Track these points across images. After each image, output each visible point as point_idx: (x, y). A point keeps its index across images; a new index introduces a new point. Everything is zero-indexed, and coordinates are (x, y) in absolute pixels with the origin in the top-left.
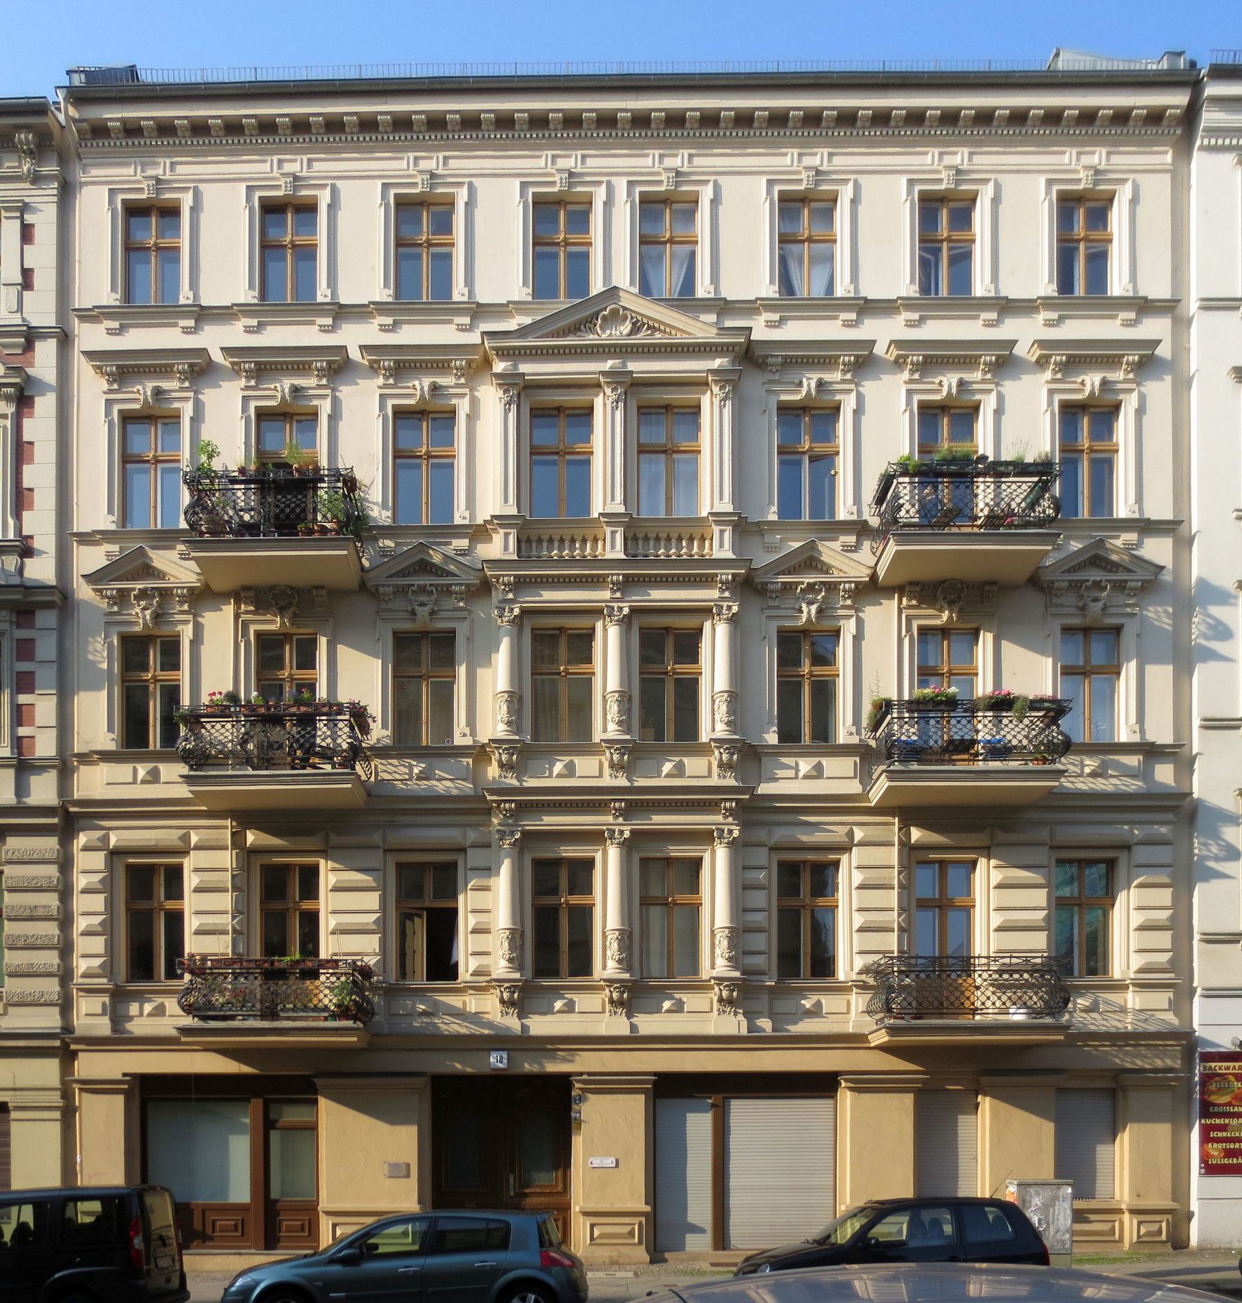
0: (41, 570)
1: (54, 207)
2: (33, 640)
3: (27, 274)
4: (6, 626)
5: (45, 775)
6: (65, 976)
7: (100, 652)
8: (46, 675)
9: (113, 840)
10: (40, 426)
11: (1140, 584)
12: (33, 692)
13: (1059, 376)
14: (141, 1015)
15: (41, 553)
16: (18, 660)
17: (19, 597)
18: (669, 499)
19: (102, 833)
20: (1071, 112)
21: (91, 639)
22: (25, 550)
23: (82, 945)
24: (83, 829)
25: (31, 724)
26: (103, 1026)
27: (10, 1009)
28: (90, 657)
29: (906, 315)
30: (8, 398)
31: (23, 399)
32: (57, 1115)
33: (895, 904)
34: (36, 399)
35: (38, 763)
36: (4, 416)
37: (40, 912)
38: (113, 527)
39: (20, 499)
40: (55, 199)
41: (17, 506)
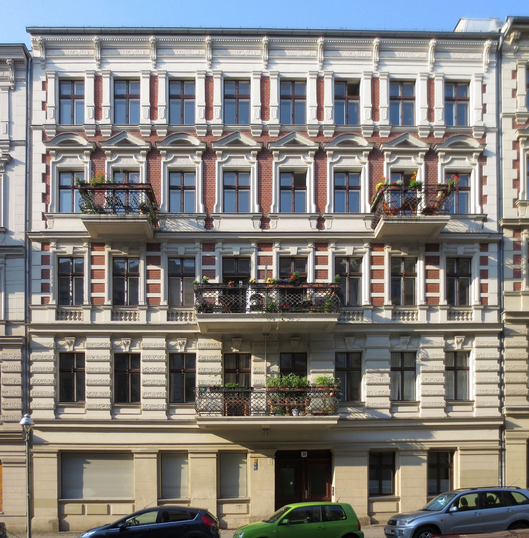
3: (484, 105)
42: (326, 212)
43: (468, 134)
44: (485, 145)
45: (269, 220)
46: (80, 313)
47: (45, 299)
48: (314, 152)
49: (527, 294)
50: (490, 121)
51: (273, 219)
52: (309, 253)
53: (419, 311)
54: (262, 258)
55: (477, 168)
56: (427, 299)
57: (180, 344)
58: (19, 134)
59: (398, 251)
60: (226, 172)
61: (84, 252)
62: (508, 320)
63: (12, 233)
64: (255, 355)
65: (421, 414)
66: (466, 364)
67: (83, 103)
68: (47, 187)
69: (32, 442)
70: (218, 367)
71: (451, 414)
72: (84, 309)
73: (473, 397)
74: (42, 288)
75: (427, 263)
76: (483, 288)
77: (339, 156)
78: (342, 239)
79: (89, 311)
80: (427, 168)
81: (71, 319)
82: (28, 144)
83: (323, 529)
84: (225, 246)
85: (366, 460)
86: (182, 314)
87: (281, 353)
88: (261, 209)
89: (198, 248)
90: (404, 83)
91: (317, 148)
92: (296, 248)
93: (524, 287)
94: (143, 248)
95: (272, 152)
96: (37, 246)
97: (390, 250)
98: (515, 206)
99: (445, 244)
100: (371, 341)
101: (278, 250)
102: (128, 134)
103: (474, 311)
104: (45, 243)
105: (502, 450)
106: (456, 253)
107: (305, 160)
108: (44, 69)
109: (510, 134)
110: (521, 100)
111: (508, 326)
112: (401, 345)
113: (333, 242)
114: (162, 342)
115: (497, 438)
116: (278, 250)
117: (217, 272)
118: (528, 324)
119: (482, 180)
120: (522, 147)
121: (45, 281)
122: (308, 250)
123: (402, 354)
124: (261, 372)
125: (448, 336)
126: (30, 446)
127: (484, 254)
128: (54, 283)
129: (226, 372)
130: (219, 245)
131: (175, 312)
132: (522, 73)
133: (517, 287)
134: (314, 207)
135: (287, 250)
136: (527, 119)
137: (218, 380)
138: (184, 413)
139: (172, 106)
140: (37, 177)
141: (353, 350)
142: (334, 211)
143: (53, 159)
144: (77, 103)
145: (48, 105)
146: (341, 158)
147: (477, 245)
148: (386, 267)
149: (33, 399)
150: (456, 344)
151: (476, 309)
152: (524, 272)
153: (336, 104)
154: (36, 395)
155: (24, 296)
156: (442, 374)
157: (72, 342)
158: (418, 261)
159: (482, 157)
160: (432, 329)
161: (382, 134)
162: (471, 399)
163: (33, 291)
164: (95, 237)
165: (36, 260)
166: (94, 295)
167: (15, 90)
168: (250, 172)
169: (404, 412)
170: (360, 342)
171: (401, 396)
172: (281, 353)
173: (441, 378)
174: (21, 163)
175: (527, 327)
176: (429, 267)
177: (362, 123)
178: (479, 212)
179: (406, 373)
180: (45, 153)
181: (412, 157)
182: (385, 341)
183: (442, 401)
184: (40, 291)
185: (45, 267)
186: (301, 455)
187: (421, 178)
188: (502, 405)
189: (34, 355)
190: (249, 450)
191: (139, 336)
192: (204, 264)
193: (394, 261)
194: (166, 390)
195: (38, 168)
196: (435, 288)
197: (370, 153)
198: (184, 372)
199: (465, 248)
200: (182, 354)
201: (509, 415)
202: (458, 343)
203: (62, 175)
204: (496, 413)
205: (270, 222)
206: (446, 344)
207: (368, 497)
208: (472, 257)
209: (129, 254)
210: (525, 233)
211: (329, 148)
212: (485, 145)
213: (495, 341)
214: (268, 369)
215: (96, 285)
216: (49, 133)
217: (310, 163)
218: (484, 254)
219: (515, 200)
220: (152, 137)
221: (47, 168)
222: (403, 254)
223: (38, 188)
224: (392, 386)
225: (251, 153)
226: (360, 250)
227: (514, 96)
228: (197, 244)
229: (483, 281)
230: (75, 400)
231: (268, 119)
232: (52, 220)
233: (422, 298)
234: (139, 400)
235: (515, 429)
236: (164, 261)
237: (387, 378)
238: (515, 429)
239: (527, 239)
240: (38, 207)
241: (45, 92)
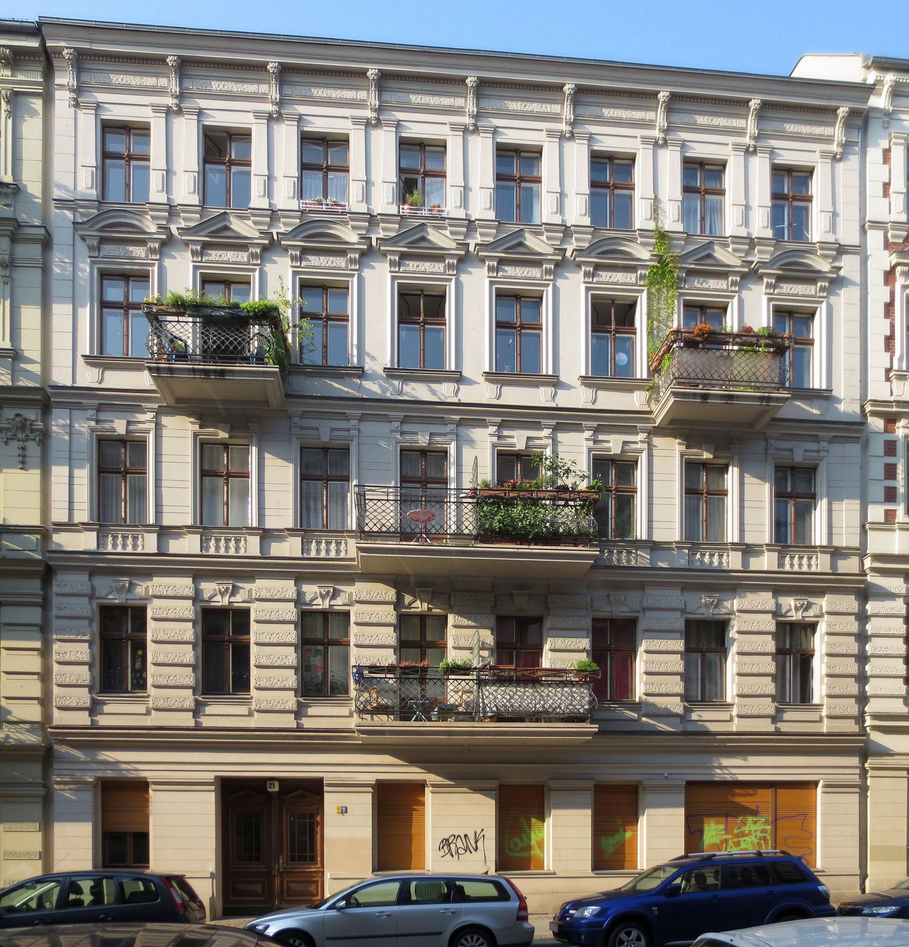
49: (906, 528)
50: (848, 235)
62: (873, 570)
63: (839, 401)
66: (809, 642)
68: (892, 326)
69: (865, 751)
70: (389, 636)
73: (733, 697)
82: (860, 250)
83: (388, 916)
85: (589, 797)
92: (124, 422)
93: (901, 516)
96: (877, 424)
98: (888, 379)
104: (891, 419)
108: (886, 128)
109: (881, 259)
110: (898, 202)
111: (871, 578)
118: (908, 576)
120: (900, 281)
121: (890, 483)
126: (864, 759)
129: (403, 645)
132: (898, 154)
133: (890, 516)
136: (906, 233)
137: (388, 658)
138: (325, 715)
140: (876, 309)
141: (621, 614)
149: (871, 679)
151: (769, 550)
152: (901, 490)
154: (875, 672)
155: (858, 507)
158: (730, 468)
162: (729, 700)
163: (870, 498)
165: (877, 447)
167: (840, 160)
173: (769, 665)
174: (853, 283)
175: (905, 582)
177: (638, 225)
185: (890, 460)
186: (274, 792)
187: (732, 327)
188: (862, 713)
190: (431, 778)
195: (878, 294)
201: (875, 728)
202: (797, 609)
204: (851, 726)
208: (818, 465)
210: (904, 427)
213: (850, 603)
219: (888, 371)
222: (707, 456)
223: (878, 327)
224: (686, 677)
227: (886, 194)
230: (130, 689)
234: (247, 688)
239: (906, 436)
240: (878, 359)
241: (887, 166)
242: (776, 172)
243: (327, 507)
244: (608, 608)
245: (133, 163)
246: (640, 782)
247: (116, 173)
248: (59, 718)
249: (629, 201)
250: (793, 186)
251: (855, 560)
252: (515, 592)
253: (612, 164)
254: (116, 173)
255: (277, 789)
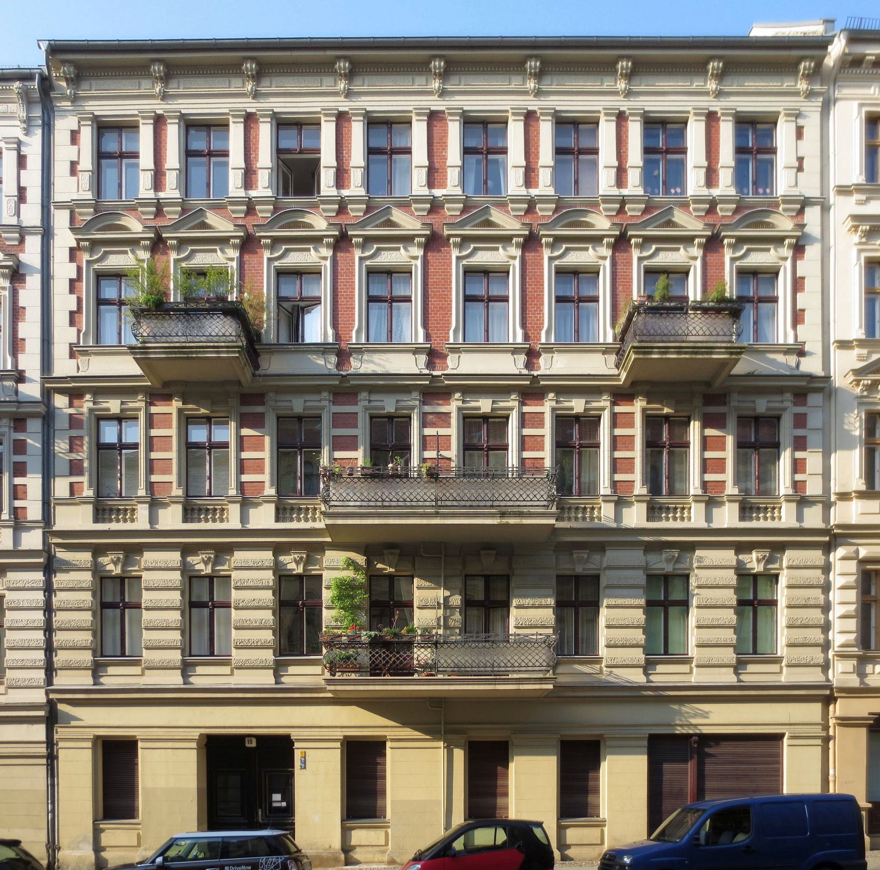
0: (811, 366)
1: (818, 115)
2: (805, 414)
3: (800, 160)
4: (6, 429)
5: (814, 507)
6: (826, 646)
7: (854, 424)
8: (813, 438)
9: (863, 552)
10: (30, 295)
11: (870, 382)
12: (805, 450)
13: (864, 240)
14: (874, 673)
15: (811, 354)
16: (14, 454)
17: (804, 384)
18: (577, 331)
19: (855, 548)
20: (870, 57)
21: (846, 415)
22: (20, 377)
23: (837, 625)
24: (841, 545)
25: (804, 472)
26: (854, 681)
27: (9, 690)
28: (846, 427)
29: (856, 197)
30: (4, 276)
31: (16, 275)
32: (819, 742)
33: (417, 613)
34: (27, 278)
35: (28, 525)
36: (4, 288)
37: (812, 602)
38: (863, 337)
39: (16, 346)
40: (820, 109)
41: (14, 348)
42: (543, 340)
43: (772, 207)
44: (804, 226)
45: (539, 355)
46: (134, 510)
47: (76, 486)
48: (704, 240)
50: (809, 187)
51: (546, 352)
52: (512, 409)
53: (693, 505)
54: (530, 416)
55: (788, 264)
56: (704, 485)
57: (295, 561)
58: (31, 215)
59: (658, 406)
60: (372, 272)
61: (139, 410)
64: (418, 577)
65: (697, 677)
67: (226, 164)
68: (79, 300)
71: (746, 678)
72: (139, 502)
74: (71, 468)
75: (704, 426)
76: (798, 466)
77: (564, 246)
78: (475, 386)
79: (238, 506)
80: (614, 264)
81: (207, 521)
84: (374, 397)
86: (300, 509)
87: (466, 576)
88: (526, 337)
89: (325, 400)
90: (669, 126)
91: (527, 233)
92: (119, 401)
94: (698, 401)
95: (449, 240)
97: (644, 404)
99: (271, 395)
100: (612, 556)
101: (460, 404)
102: (207, 214)
103: (784, 505)
105: (51, 758)
106: (755, 409)
107: (408, 254)
112: (661, 563)
113: (458, 391)
114: (267, 556)
115: (43, 738)
116: (554, 404)
117: (360, 439)
119: (798, 284)
122: (602, 404)
123: (667, 578)
124: (429, 604)
125: (741, 548)
127: (800, 410)
128: (90, 458)
130: (363, 395)
131: (108, 507)
134: (520, 332)
135: (104, 405)
138: (306, 674)
139: (371, 166)
142: (555, 340)
143: (85, 257)
144: (215, 164)
145: (79, 168)
146: (567, 249)
147: (788, 396)
148: (637, 431)
150: (754, 561)
151: (787, 501)
153: (646, 162)
156: (732, 610)
157: (119, 559)
158: (692, 423)
159: (799, 249)
160: (715, 538)
161: (721, 210)
164: (158, 385)
166: (245, 478)
168: (508, 273)
169: (666, 675)
170: (596, 557)
171: (660, 647)
172: (466, 576)
173: (729, 616)
176: (709, 432)
178: (791, 340)
179: (760, 609)
180: (74, 244)
181: (681, 247)
182: (636, 557)
183: (729, 655)
184: (67, 472)
189: (60, 579)
191: (229, 549)
192: (335, 426)
193: (652, 422)
194: (274, 635)
195: (63, 270)
196: (720, 465)
197: (615, 240)
198: (304, 605)
199: (768, 402)
200: (300, 577)
202: (758, 561)
203: (103, 283)
205: (449, 358)
206: (739, 562)
207: (342, 821)
209: (212, 412)
211: (546, 236)
212: (803, 226)
214: (446, 599)
215: (160, 462)
216: (80, 214)
217: (416, 258)
218: (800, 410)
220: (249, 218)
221: (79, 269)
222: (666, 410)
223: (63, 302)
225: (514, 241)
226: (131, 405)
228: (415, 395)
229: (799, 455)
231: (536, 186)
232: (87, 358)
233: (788, 483)
235: (73, 723)
236: (271, 421)
237: (639, 615)
238: (73, 723)
242: (650, 126)
243: (210, 478)
244: (568, 566)
245: (213, 159)
246: (602, 735)
247: (198, 172)
248: (62, 680)
249: (681, 165)
250: (757, 137)
251: (818, 509)
252: (482, 552)
253: (665, 130)
254: (110, 173)
255: (254, 745)
